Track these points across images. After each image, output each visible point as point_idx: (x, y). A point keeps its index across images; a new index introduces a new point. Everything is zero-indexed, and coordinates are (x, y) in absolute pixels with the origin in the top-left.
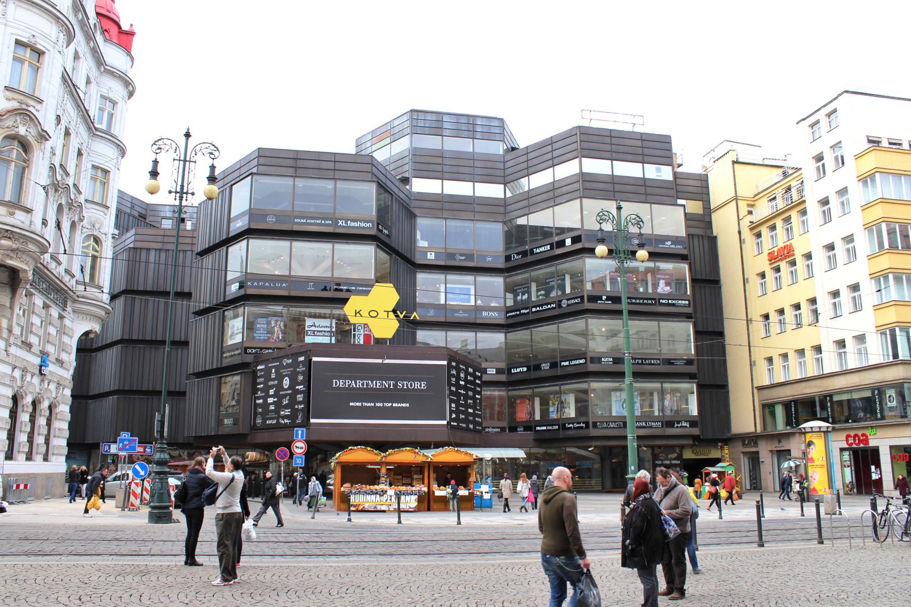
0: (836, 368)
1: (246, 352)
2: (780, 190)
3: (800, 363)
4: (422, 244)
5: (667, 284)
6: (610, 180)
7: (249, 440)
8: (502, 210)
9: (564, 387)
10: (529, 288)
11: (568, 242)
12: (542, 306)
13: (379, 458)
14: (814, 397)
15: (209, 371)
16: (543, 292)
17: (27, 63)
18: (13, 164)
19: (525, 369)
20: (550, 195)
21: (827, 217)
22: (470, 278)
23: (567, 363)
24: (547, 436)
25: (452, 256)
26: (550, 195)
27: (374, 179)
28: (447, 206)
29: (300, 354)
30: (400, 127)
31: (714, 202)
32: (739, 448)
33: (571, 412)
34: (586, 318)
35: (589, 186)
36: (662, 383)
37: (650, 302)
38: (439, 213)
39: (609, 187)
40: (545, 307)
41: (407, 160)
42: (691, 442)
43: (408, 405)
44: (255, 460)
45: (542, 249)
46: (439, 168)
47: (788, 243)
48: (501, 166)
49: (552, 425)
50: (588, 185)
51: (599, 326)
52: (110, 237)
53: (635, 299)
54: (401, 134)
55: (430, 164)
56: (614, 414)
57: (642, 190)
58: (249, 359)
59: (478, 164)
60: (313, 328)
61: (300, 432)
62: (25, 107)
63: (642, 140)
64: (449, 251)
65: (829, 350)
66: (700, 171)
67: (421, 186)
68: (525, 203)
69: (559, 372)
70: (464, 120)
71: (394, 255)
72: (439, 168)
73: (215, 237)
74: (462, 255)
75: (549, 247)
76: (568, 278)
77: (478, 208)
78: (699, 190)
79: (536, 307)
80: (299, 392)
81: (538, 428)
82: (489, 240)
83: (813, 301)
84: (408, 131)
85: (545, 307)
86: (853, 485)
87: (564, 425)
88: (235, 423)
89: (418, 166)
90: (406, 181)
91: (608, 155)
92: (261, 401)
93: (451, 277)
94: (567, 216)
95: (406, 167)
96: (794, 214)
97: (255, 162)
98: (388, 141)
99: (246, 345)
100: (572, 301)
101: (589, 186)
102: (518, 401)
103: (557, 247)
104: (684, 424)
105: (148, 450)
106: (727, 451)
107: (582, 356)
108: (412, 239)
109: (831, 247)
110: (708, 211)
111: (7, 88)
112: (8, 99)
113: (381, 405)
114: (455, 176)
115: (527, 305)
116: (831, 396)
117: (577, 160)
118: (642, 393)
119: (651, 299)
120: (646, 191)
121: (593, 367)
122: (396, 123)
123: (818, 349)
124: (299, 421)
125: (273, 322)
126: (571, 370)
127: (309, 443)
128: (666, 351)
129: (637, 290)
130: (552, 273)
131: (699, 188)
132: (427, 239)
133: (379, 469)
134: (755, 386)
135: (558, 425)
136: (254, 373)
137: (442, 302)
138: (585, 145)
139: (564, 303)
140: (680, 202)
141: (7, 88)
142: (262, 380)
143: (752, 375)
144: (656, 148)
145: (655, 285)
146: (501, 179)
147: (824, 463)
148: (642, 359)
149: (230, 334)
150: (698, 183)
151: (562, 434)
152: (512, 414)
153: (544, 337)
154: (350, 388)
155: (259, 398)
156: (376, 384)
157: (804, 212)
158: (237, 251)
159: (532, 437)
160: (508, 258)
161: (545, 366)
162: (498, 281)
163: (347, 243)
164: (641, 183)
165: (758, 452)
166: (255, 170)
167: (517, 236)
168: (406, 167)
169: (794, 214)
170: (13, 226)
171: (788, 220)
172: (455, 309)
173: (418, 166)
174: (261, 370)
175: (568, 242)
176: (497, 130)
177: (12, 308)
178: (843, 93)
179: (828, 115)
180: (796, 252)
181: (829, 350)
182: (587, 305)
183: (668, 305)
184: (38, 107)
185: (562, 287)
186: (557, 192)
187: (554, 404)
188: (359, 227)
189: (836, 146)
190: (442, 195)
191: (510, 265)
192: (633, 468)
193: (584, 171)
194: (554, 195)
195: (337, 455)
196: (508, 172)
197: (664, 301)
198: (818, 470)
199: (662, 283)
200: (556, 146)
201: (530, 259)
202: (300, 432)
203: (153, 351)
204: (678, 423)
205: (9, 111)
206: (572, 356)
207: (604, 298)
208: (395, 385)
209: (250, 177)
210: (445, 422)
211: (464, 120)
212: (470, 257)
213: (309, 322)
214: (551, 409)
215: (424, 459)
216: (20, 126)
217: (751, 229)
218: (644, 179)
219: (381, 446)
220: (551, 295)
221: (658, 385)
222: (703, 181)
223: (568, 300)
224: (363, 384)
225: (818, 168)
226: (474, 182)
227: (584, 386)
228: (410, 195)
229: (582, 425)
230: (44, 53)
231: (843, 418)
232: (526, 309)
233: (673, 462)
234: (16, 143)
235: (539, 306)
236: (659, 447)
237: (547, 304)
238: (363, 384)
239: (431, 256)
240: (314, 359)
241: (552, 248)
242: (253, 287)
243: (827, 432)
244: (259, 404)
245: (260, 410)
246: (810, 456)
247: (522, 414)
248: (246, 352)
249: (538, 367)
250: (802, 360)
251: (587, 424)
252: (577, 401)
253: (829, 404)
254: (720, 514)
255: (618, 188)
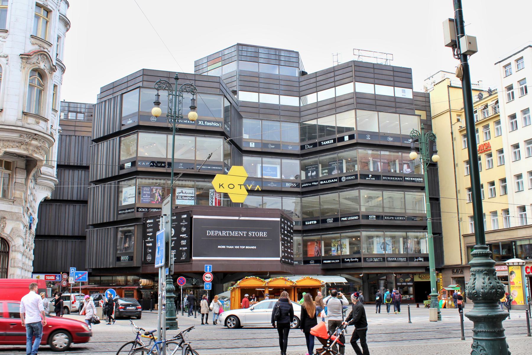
0: (519, 224)
1: (138, 211)
2: (480, 106)
3: (494, 220)
4: (245, 136)
5: (409, 167)
6: (373, 98)
7: (141, 271)
8: (297, 114)
9: (343, 235)
10: (317, 168)
11: (346, 138)
12: (327, 180)
13: (264, 284)
14: (498, 243)
15: (109, 222)
16: (326, 171)
17: (42, 18)
18: (36, 88)
19: (315, 222)
20: (333, 106)
21: (514, 126)
22: (277, 160)
23: (345, 219)
24: (331, 267)
25: (265, 145)
26: (333, 106)
27: (221, 93)
28: (262, 111)
29: (184, 213)
30: (230, 56)
31: (434, 111)
32: (450, 274)
33: (347, 251)
34: (359, 190)
35: (361, 102)
36: (406, 232)
37: (399, 179)
38: (257, 116)
39: (373, 102)
40: (329, 181)
41: (235, 79)
42: (424, 271)
43: (255, 247)
44: (146, 285)
45: (328, 142)
46: (256, 85)
47: (487, 142)
48: (297, 84)
49: (335, 260)
50: (360, 101)
51: (365, 193)
52: (57, 131)
53: (390, 177)
54: (230, 60)
55: (251, 82)
56: (375, 252)
57: (393, 104)
58: (140, 215)
59: (282, 83)
60: (181, 194)
61: (208, 267)
62: (42, 49)
63: (393, 71)
64: (264, 142)
65: (514, 212)
66: (423, 91)
67: (244, 96)
68: (315, 110)
69: (340, 224)
70: (273, 52)
71: (232, 145)
72: (256, 85)
73: (109, 129)
74: (272, 144)
75: (332, 141)
76: (344, 161)
77: (282, 113)
78: (424, 104)
79: (323, 181)
80: (183, 239)
81: (325, 262)
82: (290, 135)
83: (504, 180)
84: (236, 58)
85: (329, 181)
86: (529, 299)
87: (343, 260)
88: (131, 258)
89: (242, 83)
90: (235, 92)
91: (372, 80)
92: (150, 244)
93: (266, 159)
94: (346, 120)
95: (234, 84)
96: (491, 124)
97: (141, 79)
98: (220, 64)
99: (138, 205)
100: (349, 178)
101: (361, 102)
102: (309, 243)
103: (338, 142)
104: (420, 259)
105: (58, 278)
106: (441, 277)
107: (357, 214)
108: (241, 134)
109: (517, 146)
110: (429, 118)
111: (32, 36)
112: (33, 44)
113: (238, 247)
114: (267, 90)
115: (316, 179)
116: (515, 242)
117: (352, 83)
118: (393, 237)
119: (399, 177)
120: (395, 106)
121: (364, 222)
122: (226, 52)
123: (507, 211)
124: (183, 258)
125: (154, 190)
126: (348, 224)
127: (214, 273)
128: (410, 211)
129: (390, 171)
130: (334, 158)
131: (423, 102)
132: (251, 133)
133: (264, 291)
134: (462, 234)
135: (339, 260)
136: (145, 226)
137: (259, 176)
138: (358, 74)
139: (344, 179)
140: (417, 112)
141: (32, 36)
142: (151, 230)
143: (459, 227)
144: (402, 76)
145: (401, 169)
146: (297, 94)
147: (521, 285)
148: (394, 217)
149: (123, 198)
150: (424, 99)
151: (342, 265)
152: (305, 252)
153: (330, 201)
154: (218, 236)
155: (149, 242)
156: (235, 234)
157: (498, 122)
158: (128, 140)
159: (320, 268)
160: (303, 147)
161: (330, 221)
162: (296, 163)
163: (205, 136)
164: (393, 100)
165: (463, 277)
166: (140, 84)
167: (306, 132)
168: (234, 84)
169: (491, 124)
170: (40, 131)
171: (487, 127)
172: (269, 181)
173: (242, 83)
174: (150, 223)
175: (346, 138)
176: (294, 60)
177: (26, 184)
178: (528, 47)
179: (517, 61)
180: (492, 148)
181: (514, 212)
182: (359, 181)
183: (410, 181)
184: (49, 49)
185: (341, 169)
186: (338, 105)
187: (334, 246)
188: (213, 126)
189: (522, 81)
190: (258, 103)
191: (304, 152)
192: (434, 289)
193: (357, 91)
194: (335, 106)
195: (238, 282)
196: (302, 88)
197: (407, 179)
198: (517, 289)
199: (405, 166)
200: (337, 73)
201: (319, 148)
202: (208, 267)
203: (48, 207)
204: (417, 258)
205: (35, 53)
206: (349, 214)
207: (370, 176)
208: (247, 234)
209: (138, 89)
210: (279, 259)
211: (273, 52)
212: (277, 145)
213: (178, 190)
214: (333, 249)
215: (291, 284)
216: (41, 63)
217: (460, 132)
218: (395, 97)
219: (263, 275)
220: (333, 173)
221: (404, 234)
222: (426, 96)
223: (346, 177)
224: (226, 234)
225: (509, 95)
226: (279, 95)
227: (357, 234)
228: (238, 103)
229: (356, 260)
230: (51, 11)
231: (523, 256)
232: (316, 182)
233: (409, 284)
234: (37, 74)
235: (325, 180)
236: (401, 274)
237: (331, 179)
238: (226, 234)
239: (252, 145)
240: (194, 217)
241: (335, 142)
242: (142, 166)
243: (523, 265)
244: (149, 247)
245: (150, 251)
246: (512, 281)
247: (312, 252)
248: (138, 211)
249: (324, 221)
250: (495, 218)
251: (360, 259)
252: (350, 244)
253: (514, 247)
254: (410, 319)
255: (378, 103)
